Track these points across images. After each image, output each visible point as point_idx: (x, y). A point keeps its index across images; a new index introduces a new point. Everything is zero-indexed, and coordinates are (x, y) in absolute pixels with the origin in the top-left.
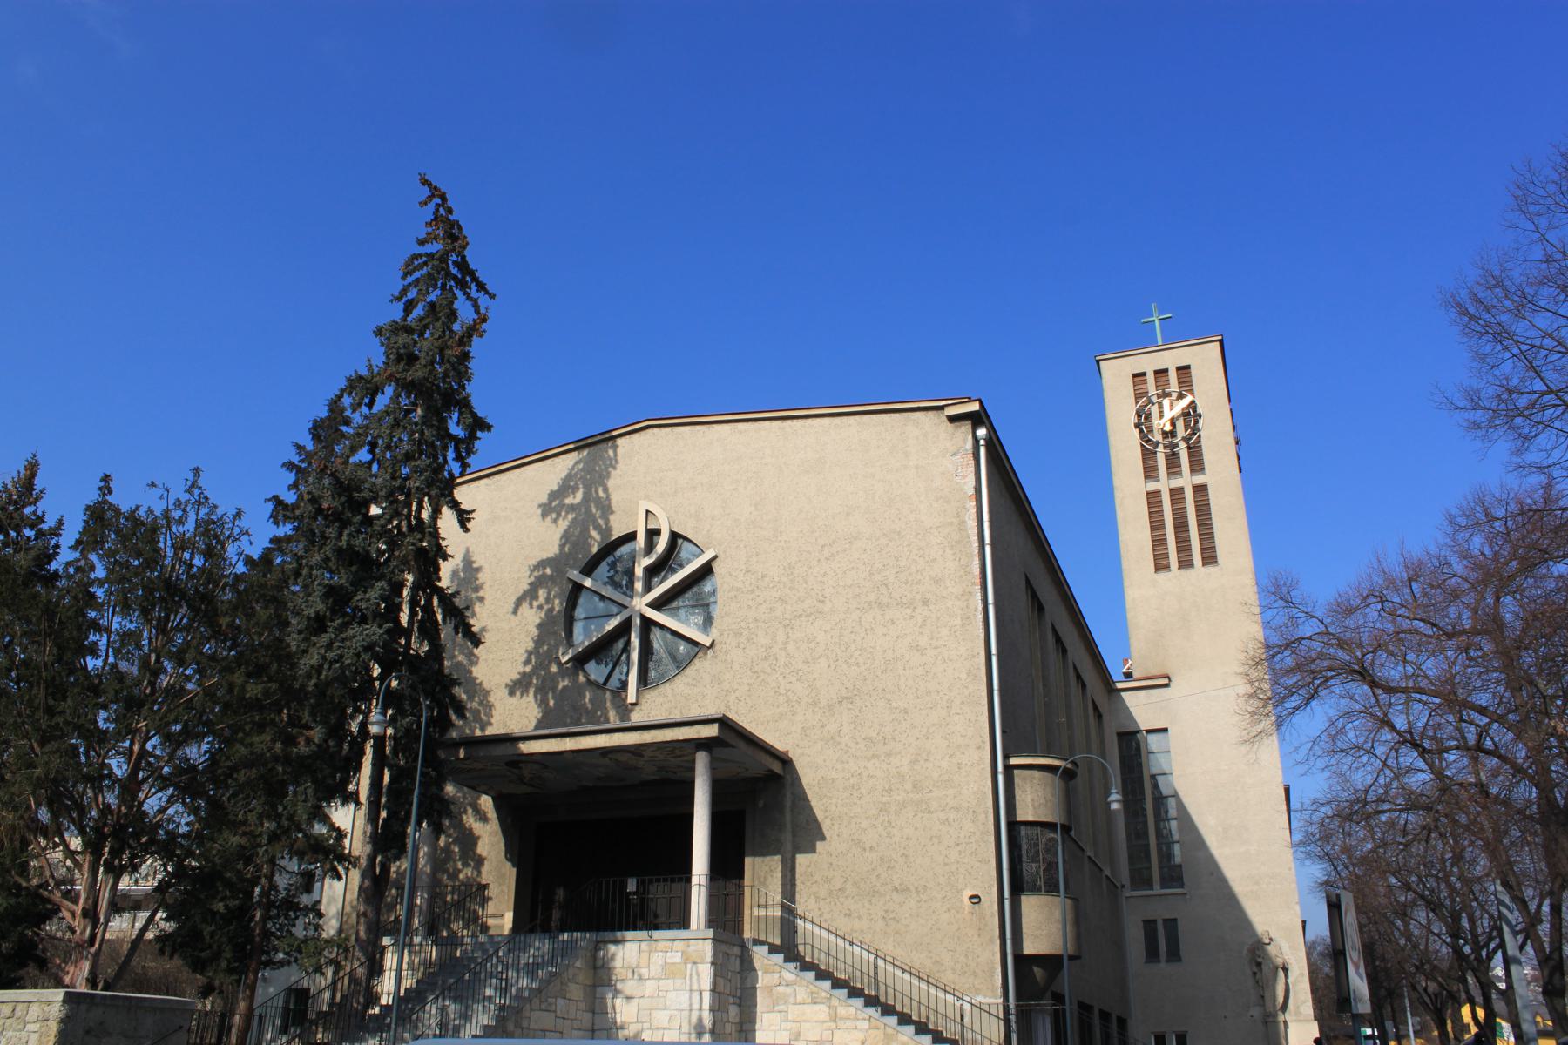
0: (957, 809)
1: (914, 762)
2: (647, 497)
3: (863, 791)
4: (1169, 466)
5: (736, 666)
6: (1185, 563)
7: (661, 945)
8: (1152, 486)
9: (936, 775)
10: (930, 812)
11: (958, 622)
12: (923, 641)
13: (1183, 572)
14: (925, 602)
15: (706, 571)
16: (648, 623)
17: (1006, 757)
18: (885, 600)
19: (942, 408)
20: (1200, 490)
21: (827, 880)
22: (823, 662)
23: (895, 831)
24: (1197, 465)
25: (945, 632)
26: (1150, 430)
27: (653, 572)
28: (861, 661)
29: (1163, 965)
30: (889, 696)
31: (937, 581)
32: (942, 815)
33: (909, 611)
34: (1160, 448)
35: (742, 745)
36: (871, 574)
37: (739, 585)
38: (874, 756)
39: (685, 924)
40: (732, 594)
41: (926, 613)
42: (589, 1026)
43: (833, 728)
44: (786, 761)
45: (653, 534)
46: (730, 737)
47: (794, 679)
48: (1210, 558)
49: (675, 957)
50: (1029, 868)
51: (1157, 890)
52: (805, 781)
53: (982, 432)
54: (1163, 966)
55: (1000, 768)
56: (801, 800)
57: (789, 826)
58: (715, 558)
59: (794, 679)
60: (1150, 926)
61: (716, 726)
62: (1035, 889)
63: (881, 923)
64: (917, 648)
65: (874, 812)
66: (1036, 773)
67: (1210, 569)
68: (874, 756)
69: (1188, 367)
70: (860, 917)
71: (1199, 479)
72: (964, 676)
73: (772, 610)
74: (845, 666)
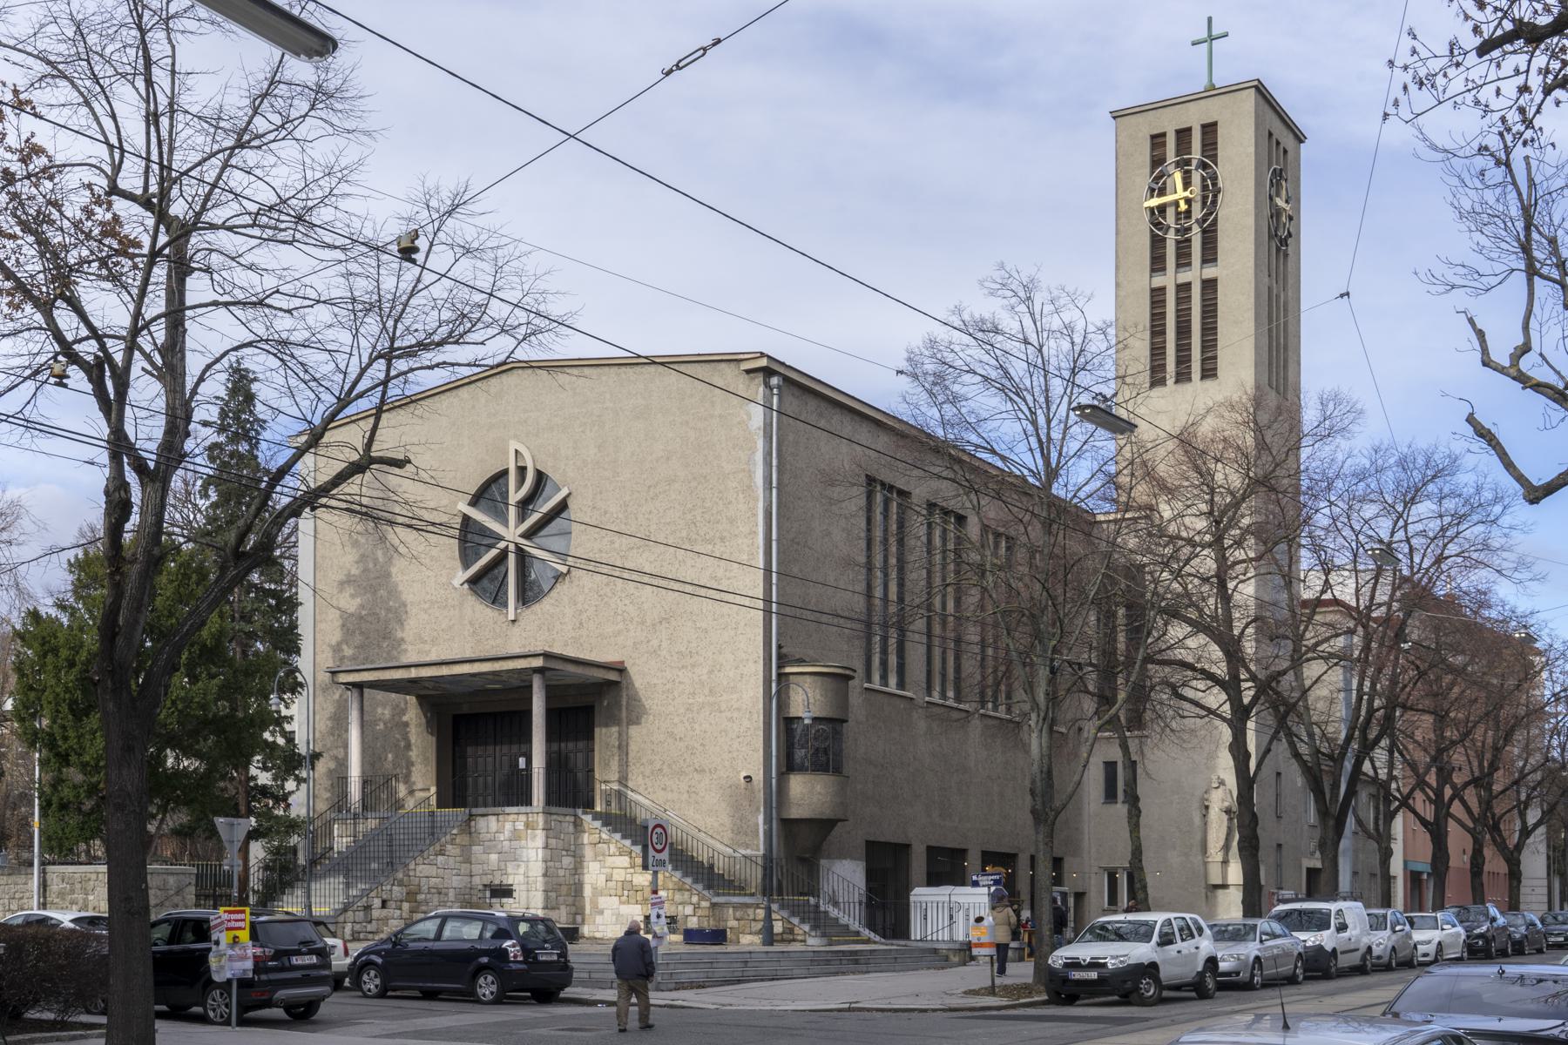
0: (738, 709)
1: (711, 672)
2: (516, 437)
4: (1178, 256)
6: (1183, 376)
7: (511, 817)
8: (1158, 281)
13: (1180, 387)
14: (722, 539)
15: (563, 506)
16: (520, 552)
17: (779, 667)
20: (1210, 285)
21: (651, 762)
24: (1210, 256)
26: (1204, 188)
27: (525, 505)
31: (732, 521)
32: (729, 714)
34: (1172, 231)
35: (571, 668)
43: (655, 643)
44: (621, 669)
45: (522, 471)
48: (1209, 372)
49: (520, 826)
50: (799, 754)
52: (637, 685)
53: (774, 381)
56: (634, 699)
62: (802, 769)
63: (686, 795)
66: (808, 679)
67: (1208, 383)
69: (1215, 124)
71: (1209, 272)
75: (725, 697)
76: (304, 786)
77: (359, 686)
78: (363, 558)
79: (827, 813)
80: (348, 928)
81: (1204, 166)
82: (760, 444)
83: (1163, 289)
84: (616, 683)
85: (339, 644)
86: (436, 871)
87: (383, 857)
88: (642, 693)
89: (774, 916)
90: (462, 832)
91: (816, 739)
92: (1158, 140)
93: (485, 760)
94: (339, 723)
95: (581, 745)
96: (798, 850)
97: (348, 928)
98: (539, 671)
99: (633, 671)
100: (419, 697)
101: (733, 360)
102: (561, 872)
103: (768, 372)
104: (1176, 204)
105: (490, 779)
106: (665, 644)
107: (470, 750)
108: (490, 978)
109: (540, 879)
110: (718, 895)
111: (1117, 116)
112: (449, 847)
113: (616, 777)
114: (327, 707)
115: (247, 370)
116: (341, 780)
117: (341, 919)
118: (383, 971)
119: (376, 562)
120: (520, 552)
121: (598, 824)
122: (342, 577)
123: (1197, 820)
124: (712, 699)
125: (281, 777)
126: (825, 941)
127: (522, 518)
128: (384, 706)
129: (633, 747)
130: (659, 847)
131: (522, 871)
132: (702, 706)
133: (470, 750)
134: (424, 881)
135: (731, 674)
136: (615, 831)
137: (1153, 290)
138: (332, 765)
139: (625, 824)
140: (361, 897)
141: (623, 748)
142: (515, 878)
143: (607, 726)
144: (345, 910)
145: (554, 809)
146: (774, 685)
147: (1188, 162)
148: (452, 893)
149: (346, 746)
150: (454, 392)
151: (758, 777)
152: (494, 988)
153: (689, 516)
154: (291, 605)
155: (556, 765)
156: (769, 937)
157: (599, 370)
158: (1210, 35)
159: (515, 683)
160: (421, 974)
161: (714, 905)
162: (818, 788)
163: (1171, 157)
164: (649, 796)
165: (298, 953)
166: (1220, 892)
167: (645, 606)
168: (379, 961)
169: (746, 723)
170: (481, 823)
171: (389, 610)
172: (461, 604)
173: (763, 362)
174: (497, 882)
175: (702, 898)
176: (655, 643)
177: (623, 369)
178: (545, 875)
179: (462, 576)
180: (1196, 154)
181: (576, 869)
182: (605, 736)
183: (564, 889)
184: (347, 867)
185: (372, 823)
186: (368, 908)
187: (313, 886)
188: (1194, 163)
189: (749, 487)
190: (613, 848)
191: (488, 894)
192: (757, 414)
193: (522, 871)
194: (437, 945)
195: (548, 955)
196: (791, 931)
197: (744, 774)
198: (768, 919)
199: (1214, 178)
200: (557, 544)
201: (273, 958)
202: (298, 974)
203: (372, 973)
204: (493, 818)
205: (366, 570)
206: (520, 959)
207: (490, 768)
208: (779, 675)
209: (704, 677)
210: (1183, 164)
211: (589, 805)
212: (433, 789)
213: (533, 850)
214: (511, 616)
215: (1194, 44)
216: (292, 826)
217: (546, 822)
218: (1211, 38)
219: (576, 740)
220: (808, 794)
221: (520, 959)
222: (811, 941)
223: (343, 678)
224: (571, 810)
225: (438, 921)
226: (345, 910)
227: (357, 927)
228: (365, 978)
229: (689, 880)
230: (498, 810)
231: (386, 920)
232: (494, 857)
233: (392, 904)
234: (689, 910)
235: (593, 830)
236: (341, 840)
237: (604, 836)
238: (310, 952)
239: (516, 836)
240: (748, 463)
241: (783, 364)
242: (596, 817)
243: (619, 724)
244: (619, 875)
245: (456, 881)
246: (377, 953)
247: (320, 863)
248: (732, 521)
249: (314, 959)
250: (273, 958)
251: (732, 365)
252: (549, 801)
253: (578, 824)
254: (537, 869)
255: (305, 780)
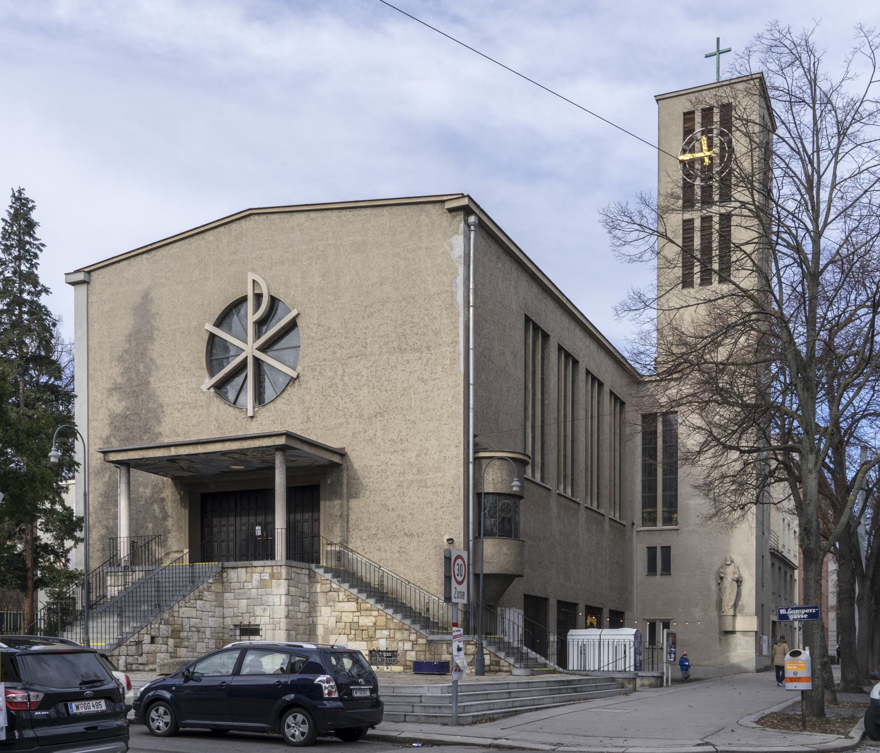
0: (442, 485)
1: (418, 455)
2: (253, 270)
3: (388, 473)
5: (313, 392)
7: (258, 569)
9: (431, 464)
10: (427, 487)
11: (448, 362)
12: (426, 376)
14: (428, 348)
15: (292, 325)
18: (404, 346)
19: (443, 202)
21: (368, 529)
22: (366, 389)
23: (406, 499)
25: (439, 369)
26: (722, 149)
27: (261, 324)
28: (388, 388)
29: (658, 577)
30: (404, 412)
31: (437, 333)
32: (434, 490)
33: (418, 354)
34: (698, 182)
35: (306, 449)
36: (395, 328)
37: (313, 335)
38: (395, 451)
39: (272, 557)
40: (310, 341)
41: (428, 356)
42: (221, 614)
43: (371, 432)
44: (342, 454)
45: (258, 297)
46: (293, 443)
47: (348, 400)
49: (266, 576)
51: (660, 526)
52: (356, 466)
53: (472, 219)
54: (658, 578)
55: (471, 460)
56: (354, 479)
57: (345, 495)
58: (298, 314)
59: (348, 400)
60: (652, 551)
61: (284, 437)
63: (397, 555)
64: (423, 380)
65: (394, 487)
66: (497, 462)
68: (395, 451)
70: (385, 551)
72: (450, 399)
73: (334, 353)
74: (378, 392)
75: (431, 475)
76: (81, 546)
77: (127, 465)
78: (127, 370)
79: (511, 570)
80: (122, 660)
81: (722, 134)
82: (461, 270)
83: (691, 221)
84: (338, 465)
85: (108, 438)
86: (197, 614)
87: (151, 600)
88: (360, 473)
89: (485, 651)
90: (216, 581)
91: (502, 510)
92: (688, 116)
93: (229, 528)
94: (110, 499)
95: (307, 516)
96: (487, 597)
97: (122, 660)
98: (282, 448)
99: (352, 455)
100: (175, 479)
101: (438, 201)
102: (299, 615)
103: (467, 211)
104: (702, 160)
105: (231, 544)
106: (379, 434)
107: (216, 521)
108: (300, 717)
109: (283, 620)
110: (433, 633)
111: (659, 99)
112: (206, 593)
113: (338, 540)
114: (97, 487)
115: (26, 199)
116: (112, 540)
117: (116, 652)
118: (173, 706)
119: (138, 372)
120: (258, 362)
121: (329, 576)
122: (111, 386)
123: (714, 587)
124: (419, 477)
125: (60, 538)
126: (528, 671)
127: (258, 334)
128: (147, 481)
129: (353, 516)
130: (460, 579)
131: (267, 613)
132: (412, 482)
133: (216, 521)
134: (185, 621)
135: (436, 457)
136: (344, 582)
137: (684, 221)
138: (103, 532)
139: (346, 574)
140: (134, 633)
141: (345, 518)
142: (262, 620)
143: (330, 499)
144: (119, 645)
145: (294, 563)
146: (471, 466)
147: (711, 131)
148: (208, 631)
149: (116, 517)
150: (202, 236)
151: (459, 540)
152: (305, 728)
153: (399, 330)
154: (69, 397)
155: (291, 529)
156: (482, 670)
157: (323, 214)
158: (718, 50)
159: (257, 464)
160: (193, 703)
161: (430, 642)
162: (505, 549)
163: (698, 128)
164: (369, 554)
165: (79, 697)
166: (731, 636)
167: (363, 403)
168: (167, 695)
169: (449, 496)
170: (233, 574)
171: (149, 410)
172: (209, 405)
173: (465, 202)
174: (246, 623)
175: (420, 636)
176: (371, 432)
177: (344, 212)
178: (287, 617)
179: (209, 382)
180: (716, 128)
181: (310, 612)
182: (328, 508)
183: (301, 628)
184: (118, 608)
185: (138, 575)
186: (139, 643)
187: (91, 625)
188: (715, 132)
189: (452, 305)
190: (342, 596)
191: (238, 632)
192: (458, 242)
193: (267, 613)
194: (237, 681)
195: (361, 692)
196: (498, 663)
197: (447, 537)
198: (480, 653)
199: (730, 142)
200: (288, 355)
201: (41, 706)
202: (79, 728)
203: (162, 710)
204: (244, 570)
205: (129, 379)
206: (336, 695)
207: (232, 536)
208: (475, 459)
209: (413, 460)
210: (707, 132)
211: (318, 562)
212: (186, 551)
213: (278, 595)
214: (250, 413)
215: (707, 57)
216: (72, 577)
217: (288, 573)
218: (719, 52)
219: (303, 512)
220: (496, 554)
221: (336, 695)
222: (516, 672)
223: (114, 457)
224: (306, 565)
225: (236, 654)
226: (119, 645)
227: (130, 660)
228: (153, 714)
229: (408, 622)
230: (246, 563)
231: (155, 653)
232: (244, 603)
233: (159, 640)
234: (408, 646)
235: (325, 582)
236: (113, 590)
237: (334, 586)
238: (97, 696)
239: (263, 584)
240: (450, 285)
241: (478, 206)
242: (327, 570)
243: (340, 499)
244: (347, 618)
245: (212, 622)
246: (167, 688)
247: (95, 607)
248: (437, 333)
249: (102, 706)
250: (41, 706)
251: (437, 206)
252: (289, 557)
253: (312, 576)
254: (281, 612)
255: (82, 540)
